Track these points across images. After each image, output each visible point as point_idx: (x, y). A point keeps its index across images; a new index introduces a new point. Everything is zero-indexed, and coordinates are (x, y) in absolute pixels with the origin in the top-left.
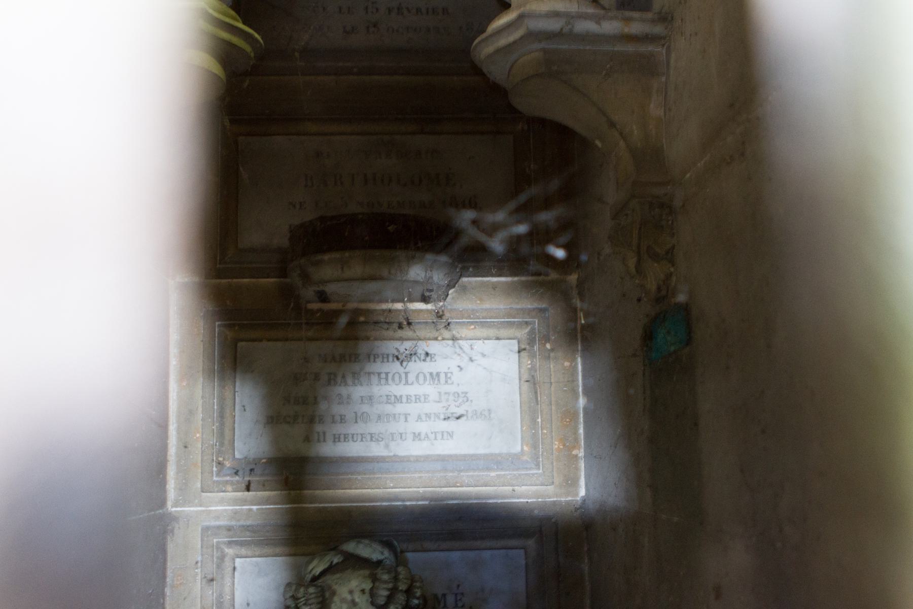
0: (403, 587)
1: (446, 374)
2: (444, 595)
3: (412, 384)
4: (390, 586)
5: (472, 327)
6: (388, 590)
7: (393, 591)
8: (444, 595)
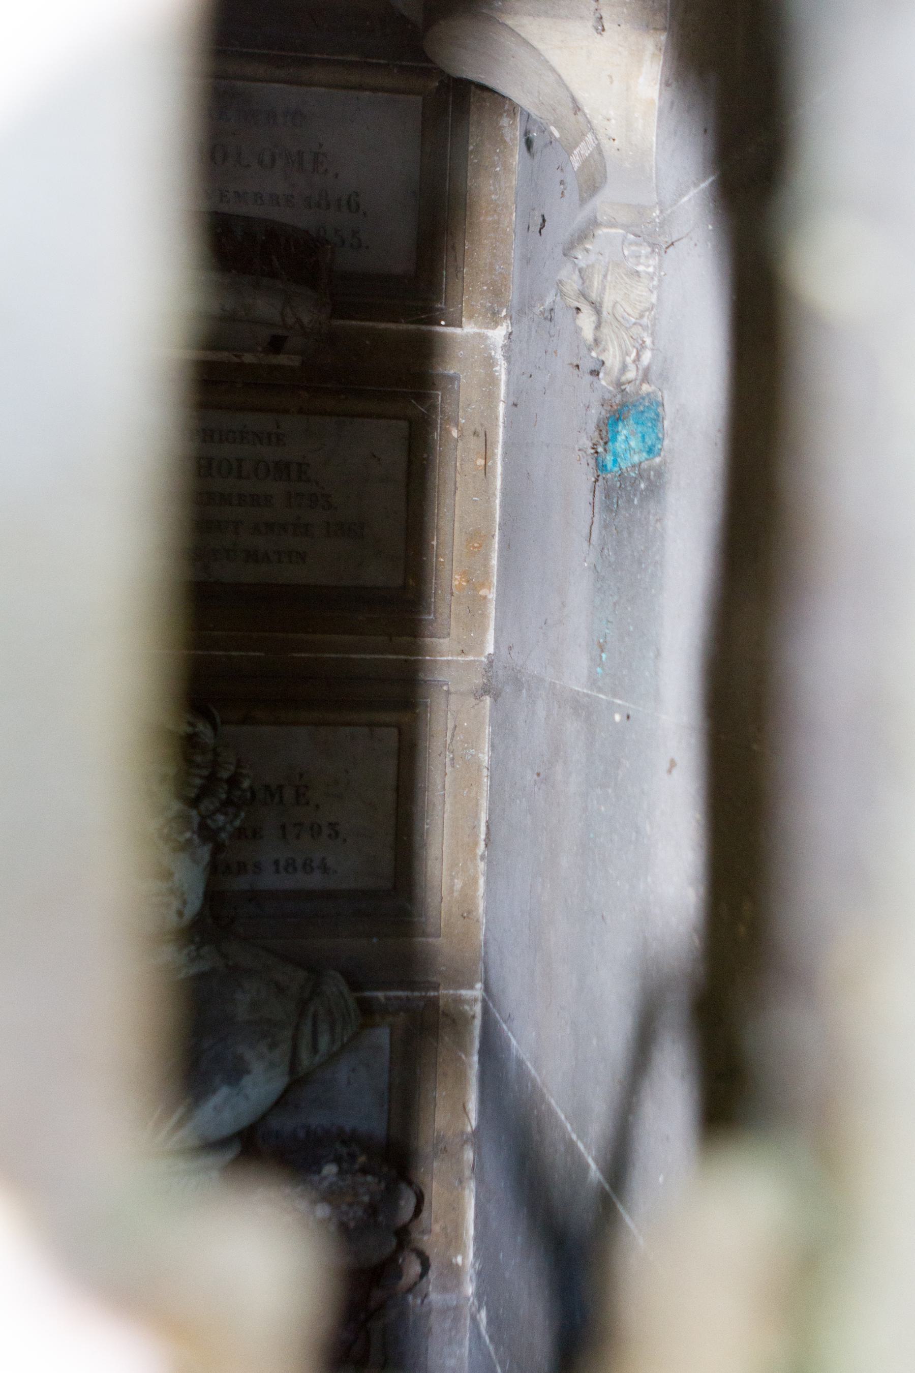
0: (225, 775)
1: (300, 465)
2: (280, 788)
4: (205, 772)
5: (343, 397)
6: (201, 777)
8: (280, 788)
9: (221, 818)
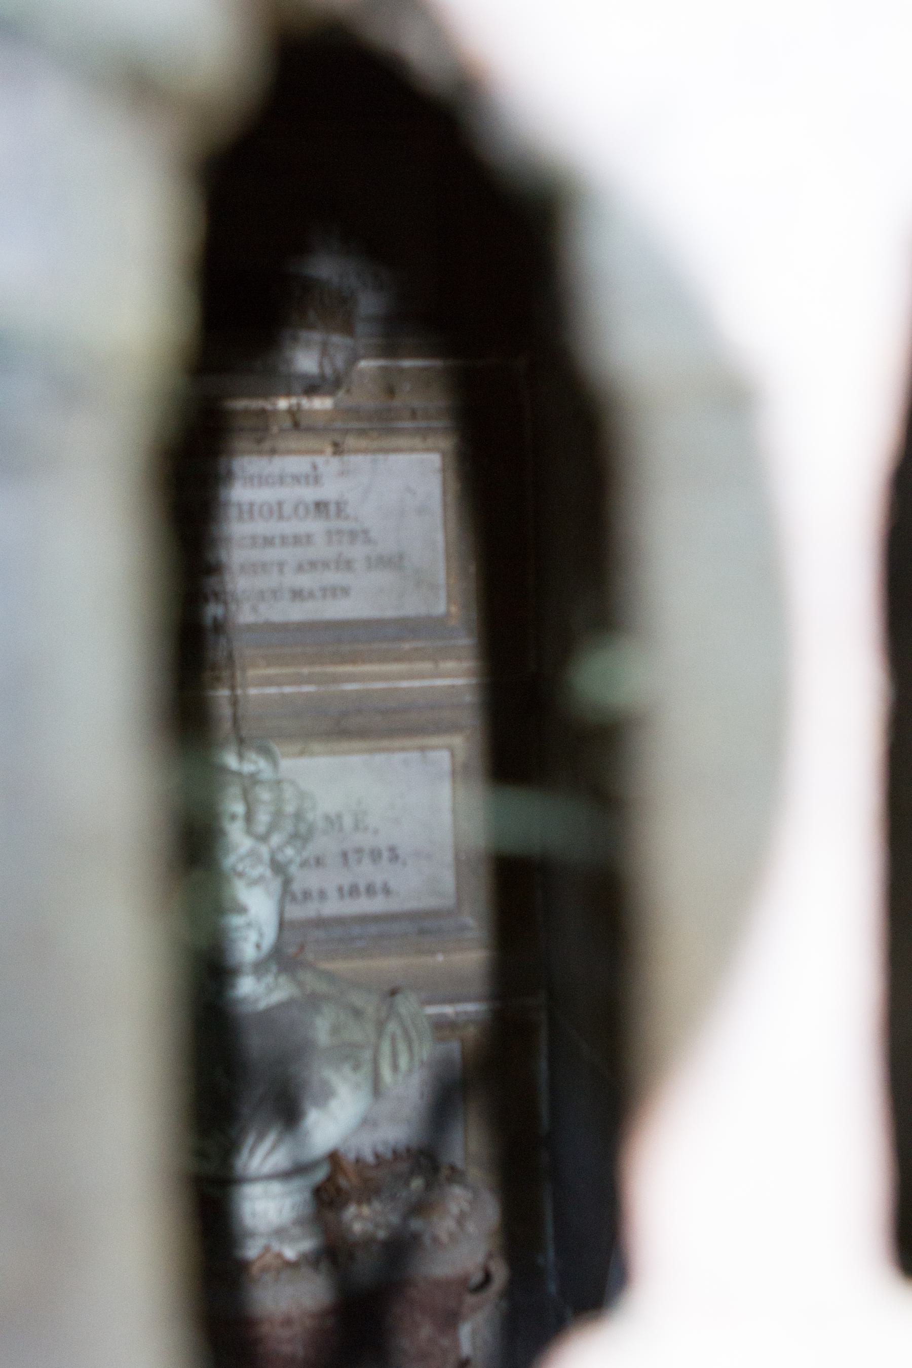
0: (290, 809)
1: (338, 504)
3: (289, 519)
7: (278, 815)
9: (290, 852)
